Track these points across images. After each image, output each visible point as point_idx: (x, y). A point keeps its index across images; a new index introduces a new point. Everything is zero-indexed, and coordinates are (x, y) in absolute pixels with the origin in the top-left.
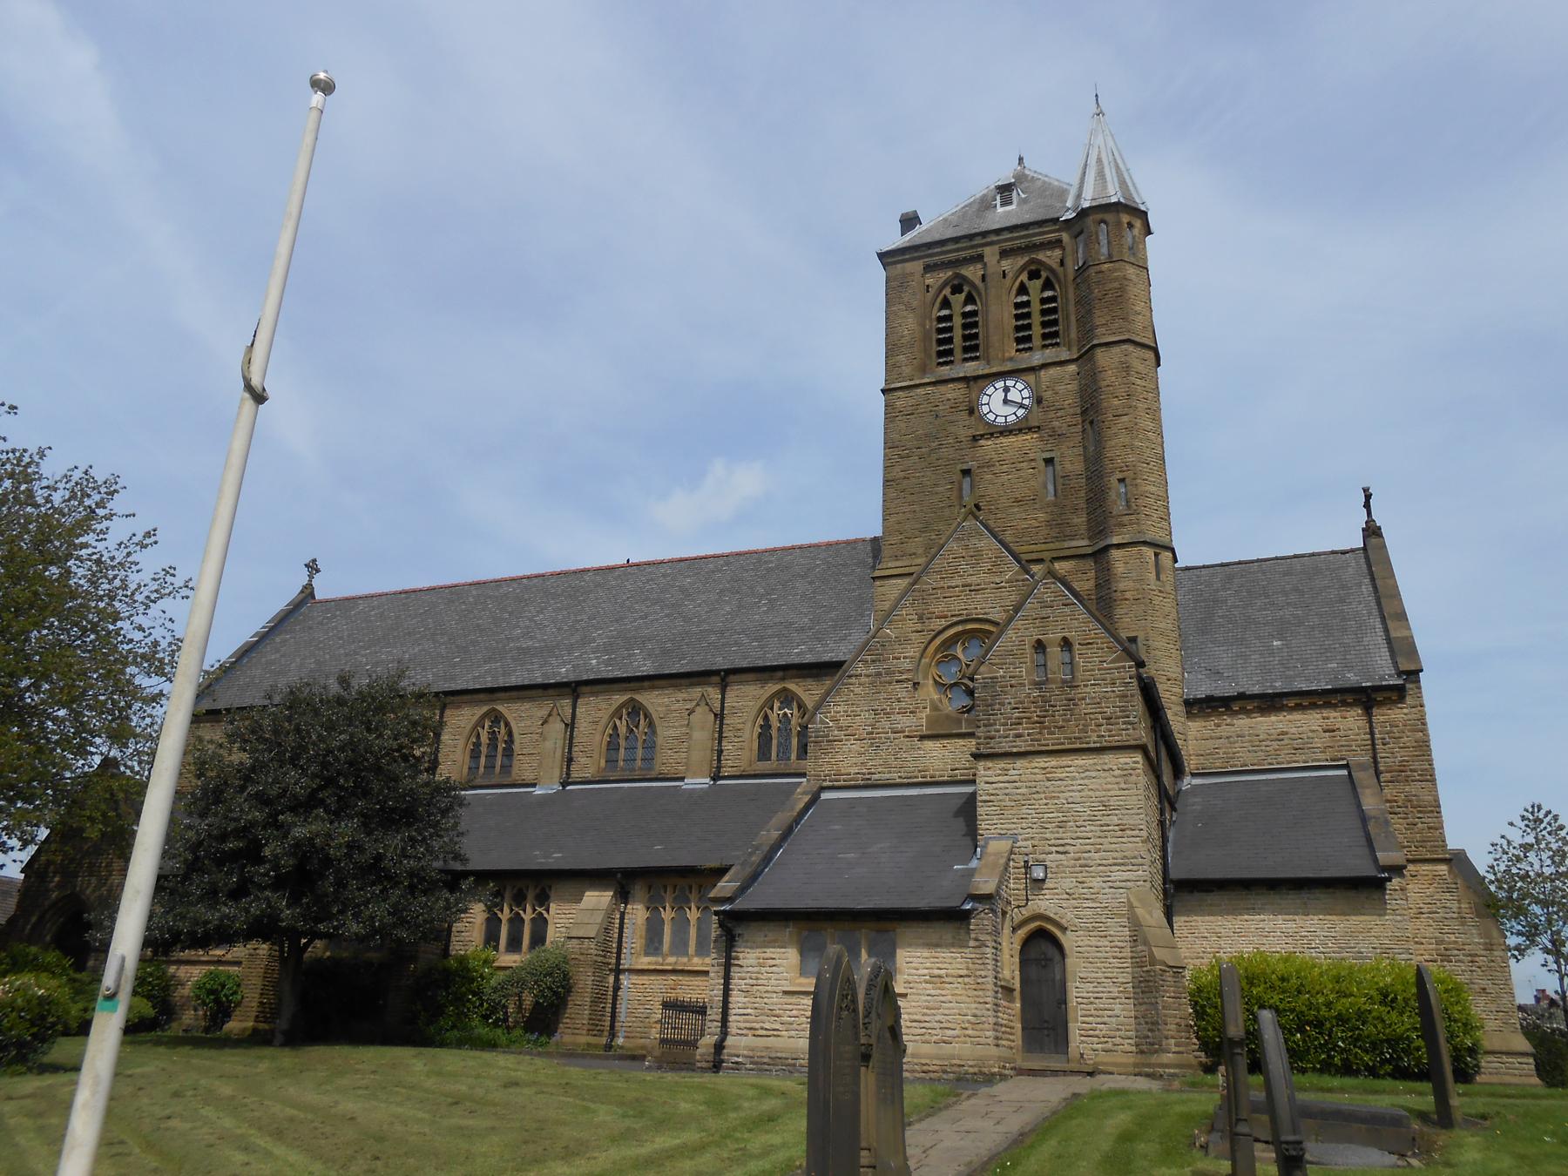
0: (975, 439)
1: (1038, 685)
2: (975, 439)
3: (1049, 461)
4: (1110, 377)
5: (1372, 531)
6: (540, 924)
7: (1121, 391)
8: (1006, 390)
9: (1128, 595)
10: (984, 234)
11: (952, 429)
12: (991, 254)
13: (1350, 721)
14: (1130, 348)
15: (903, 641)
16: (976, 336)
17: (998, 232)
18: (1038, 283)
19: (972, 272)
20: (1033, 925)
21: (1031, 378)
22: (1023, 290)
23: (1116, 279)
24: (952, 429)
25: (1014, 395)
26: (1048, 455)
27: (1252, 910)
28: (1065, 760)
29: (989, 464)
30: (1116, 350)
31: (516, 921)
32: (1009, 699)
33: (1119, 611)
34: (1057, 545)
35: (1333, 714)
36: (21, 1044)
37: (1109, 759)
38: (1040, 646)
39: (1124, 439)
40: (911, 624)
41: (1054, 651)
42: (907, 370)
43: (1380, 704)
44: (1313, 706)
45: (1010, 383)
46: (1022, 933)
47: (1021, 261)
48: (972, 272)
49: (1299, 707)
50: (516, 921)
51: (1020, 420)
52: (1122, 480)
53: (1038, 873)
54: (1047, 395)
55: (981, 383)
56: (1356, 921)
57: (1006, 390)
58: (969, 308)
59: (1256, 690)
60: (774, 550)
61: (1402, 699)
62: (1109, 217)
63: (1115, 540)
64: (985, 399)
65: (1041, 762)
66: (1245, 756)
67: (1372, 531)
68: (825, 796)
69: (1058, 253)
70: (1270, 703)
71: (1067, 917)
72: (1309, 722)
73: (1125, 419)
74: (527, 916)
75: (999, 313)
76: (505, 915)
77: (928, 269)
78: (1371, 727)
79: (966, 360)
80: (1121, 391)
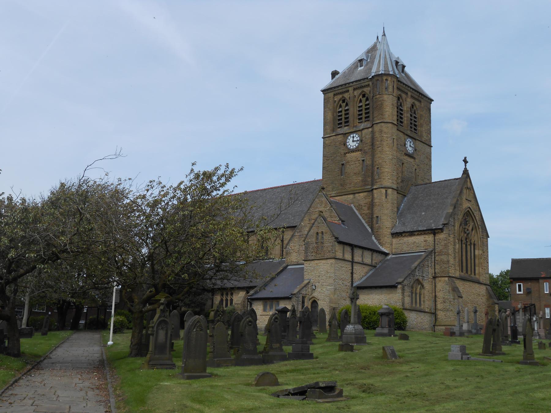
0: (345, 154)
1: (316, 243)
2: (345, 154)
3: (363, 160)
4: (377, 135)
5: (466, 172)
6: (232, 300)
7: (379, 139)
8: (353, 137)
9: (377, 204)
10: (349, 83)
11: (340, 151)
12: (351, 89)
13: (430, 238)
14: (383, 124)
15: (305, 226)
16: (348, 118)
17: (352, 82)
18: (365, 99)
19: (346, 96)
20: (313, 299)
21: (360, 133)
22: (361, 101)
23: (380, 101)
24: (340, 151)
25: (355, 139)
26: (363, 159)
27: (372, 294)
28: (320, 261)
29: (348, 162)
30: (379, 125)
31: (227, 300)
32: (311, 247)
33: (375, 208)
34: (363, 188)
35: (427, 236)
36: (119, 329)
37: (328, 260)
38: (317, 233)
39: (379, 155)
40: (307, 222)
41: (320, 234)
42: (329, 131)
43: (438, 233)
44: (421, 234)
45: (354, 135)
46: (311, 301)
47: (359, 91)
48: (346, 96)
49: (418, 235)
50: (227, 300)
51: (357, 147)
52: (378, 168)
53: (314, 287)
54: (364, 139)
55: (347, 135)
56: (391, 295)
57: (353, 137)
58: (346, 108)
59: (409, 230)
60: (308, 182)
61: (442, 232)
62: (380, 78)
63: (375, 187)
64: (348, 141)
65: (316, 262)
66: (405, 249)
67: (466, 172)
68: (289, 267)
69: (369, 89)
70: (411, 233)
71: (319, 297)
72: (419, 239)
73: (380, 148)
74: (229, 299)
75: (353, 111)
76: (224, 299)
77: (334, 95)
78: (435, 240)
79: (345, 126)
80: (379, 139)
